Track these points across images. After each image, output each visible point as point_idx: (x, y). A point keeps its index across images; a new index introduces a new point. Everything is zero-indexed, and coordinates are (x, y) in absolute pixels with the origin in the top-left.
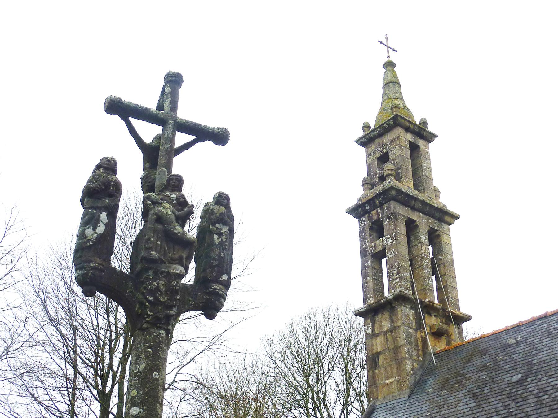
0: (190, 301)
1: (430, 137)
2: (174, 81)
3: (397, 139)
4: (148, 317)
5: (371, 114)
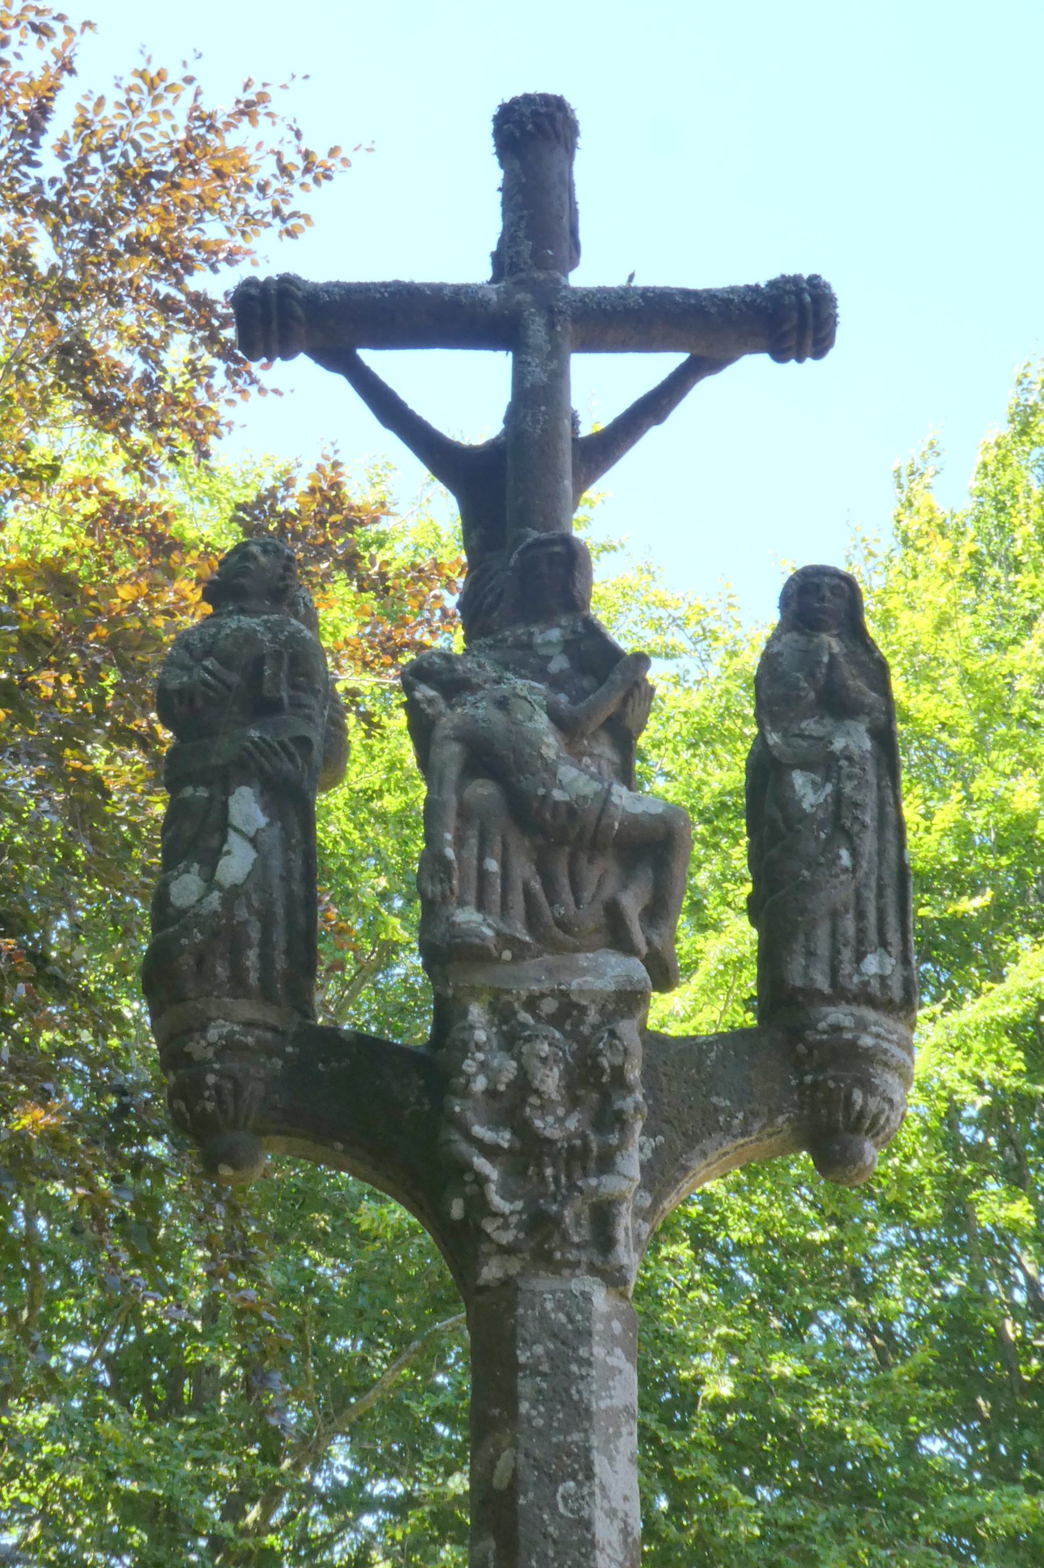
0: (717, 1109)
2: (534, 137)
4: (505, 1227)
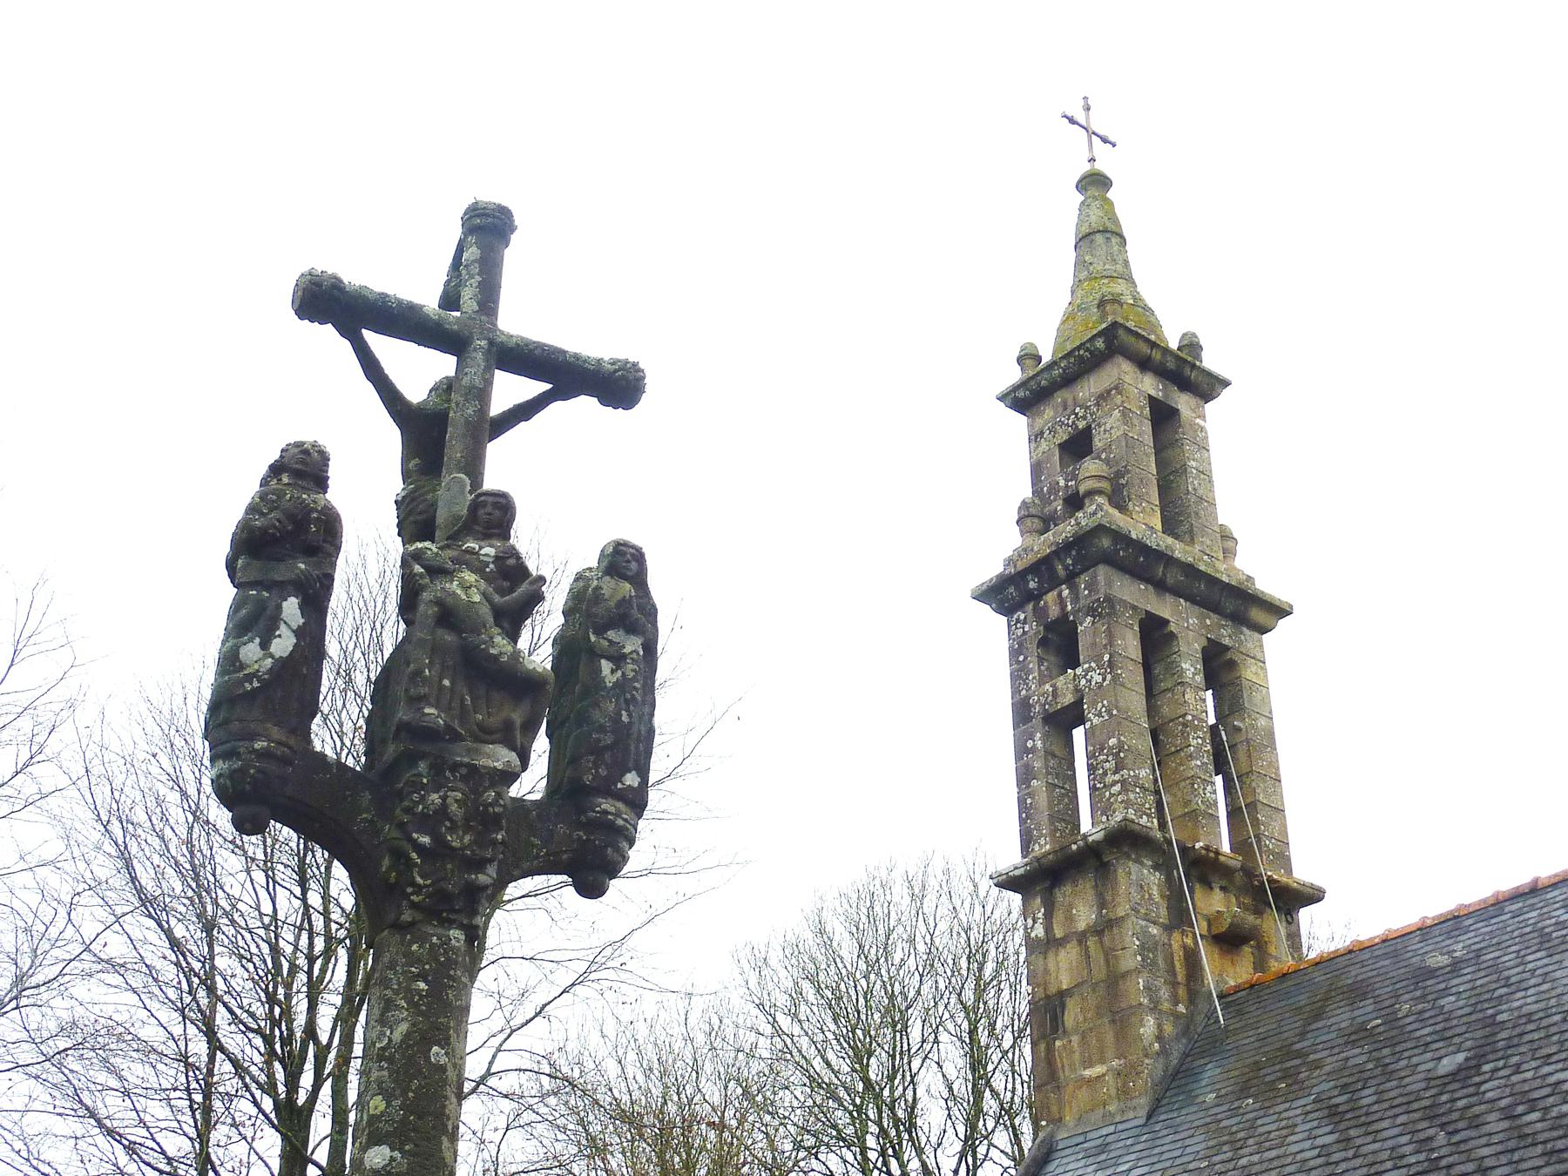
0: (533, 846)
1: (1207, 387)
2: (488, 228)
3: (1115, 392)
4: (417, 893)
5: (1043, 320)
